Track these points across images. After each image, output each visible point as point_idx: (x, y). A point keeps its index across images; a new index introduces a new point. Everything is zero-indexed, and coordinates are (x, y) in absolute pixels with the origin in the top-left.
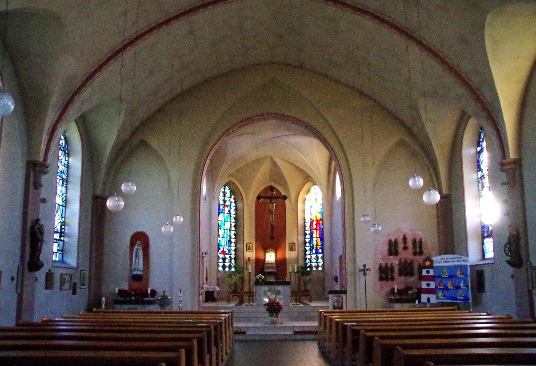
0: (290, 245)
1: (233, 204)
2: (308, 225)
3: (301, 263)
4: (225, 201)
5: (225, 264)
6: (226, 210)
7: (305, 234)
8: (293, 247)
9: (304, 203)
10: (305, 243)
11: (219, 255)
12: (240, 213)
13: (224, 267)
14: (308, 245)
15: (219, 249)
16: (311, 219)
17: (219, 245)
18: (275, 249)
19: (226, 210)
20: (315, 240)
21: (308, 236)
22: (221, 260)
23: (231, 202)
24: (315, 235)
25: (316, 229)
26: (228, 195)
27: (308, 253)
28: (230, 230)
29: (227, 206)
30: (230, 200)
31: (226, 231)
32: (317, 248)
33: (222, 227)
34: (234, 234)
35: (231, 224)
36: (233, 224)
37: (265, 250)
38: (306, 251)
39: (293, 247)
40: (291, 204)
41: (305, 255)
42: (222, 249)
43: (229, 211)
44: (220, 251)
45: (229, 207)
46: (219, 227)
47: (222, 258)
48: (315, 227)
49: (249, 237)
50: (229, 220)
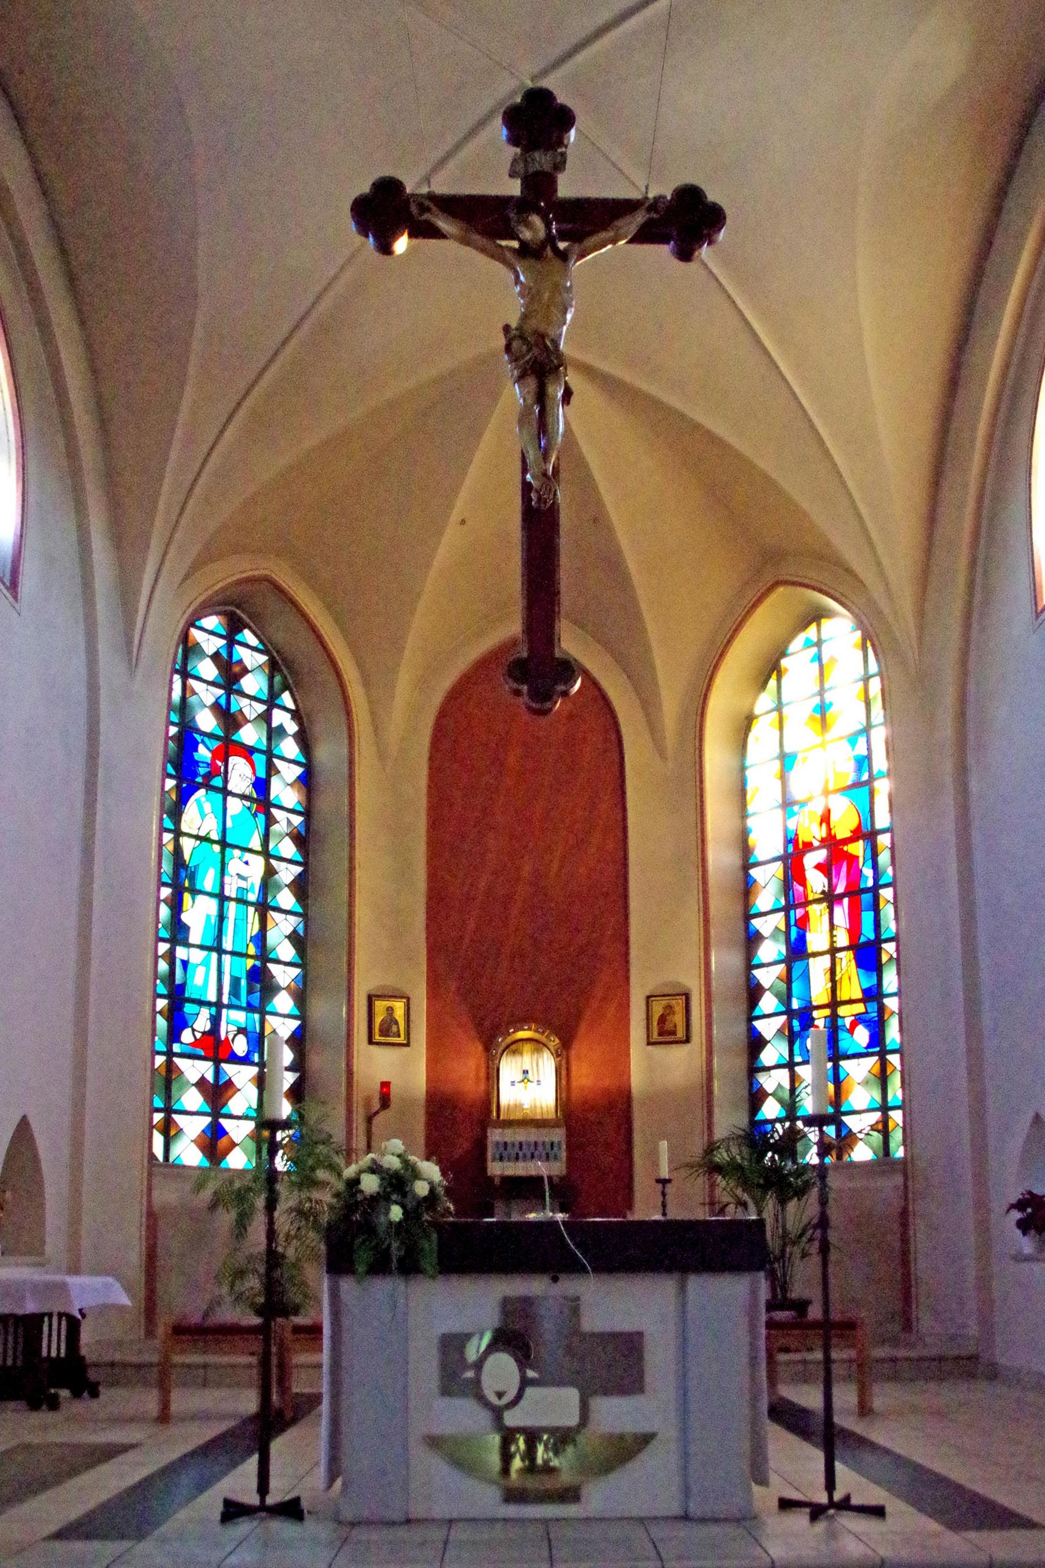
0: (658, 1009)
1: (289, 748)
2: (768, 880)
3: (729, 1120)
4: (230, 720)
5: (214, 1126)
6: (240, 775)
7: (753, 940)
8: (679, 1019)
9: (742, 746)
10: (754, 992)
11: (181, 1063)
12: (327, 803)
13: (214, 1142)
14: (768, 1003)
15: (177, 1022)
16: (792, 840)
17: (177, 995)
18: (564, 1035)
19: (240, 775)
20: (819, 967)
21: (771, 950)
22: (192, 1099)
23: (275, 733)
24: (817, 939)
25: (830, 899)
26: (254, 683)
27: (772, 1054)
28: (263, 908)
29: (248, 752)
30: (266, 717)
31: (232, 908)
32: (834, 1018)
33: (208, 881)
34: (294, 938)
35: (270, 872)
36: (287, 873)
37: (492, 1038)
38: (756, 1043)
39: (679, 1019)
40: (661, 752)
41: (754, 1069)
42: (202, 1023)
43: (262, 786)
44: (187, 1036)
45: (259, 759)
46: (182, 881)
47: (201, 1083)
48: (816, 882)
49: (389, 945)
50: (256, 844)
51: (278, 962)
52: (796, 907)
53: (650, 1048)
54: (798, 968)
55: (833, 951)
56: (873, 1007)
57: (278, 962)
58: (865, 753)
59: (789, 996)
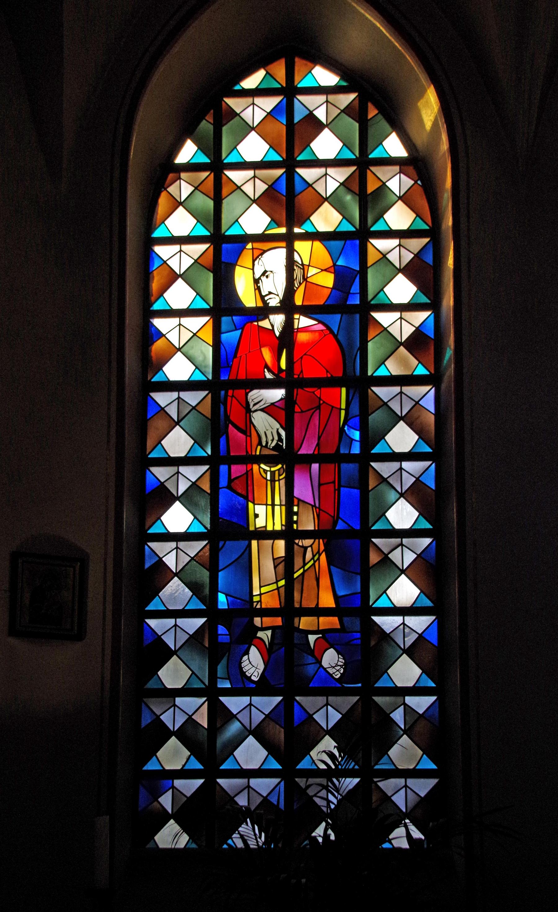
20: (265, 563)
25: (287, 457)
51: (390, 307)
52: (231, 460)
53: (12, 641)
54: (230, 551)
55: (289, 534)
56: (354, 623)
57: (390, 307)
58: (191, 672)
59: (214, 590)
